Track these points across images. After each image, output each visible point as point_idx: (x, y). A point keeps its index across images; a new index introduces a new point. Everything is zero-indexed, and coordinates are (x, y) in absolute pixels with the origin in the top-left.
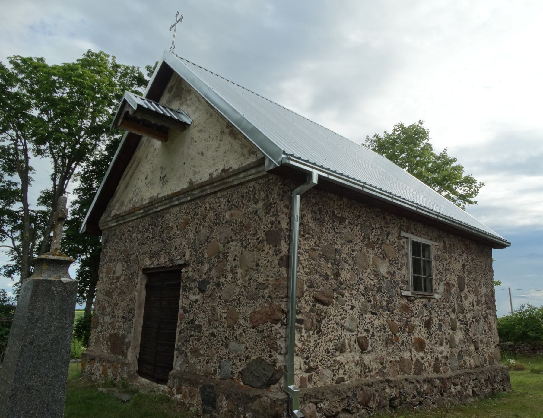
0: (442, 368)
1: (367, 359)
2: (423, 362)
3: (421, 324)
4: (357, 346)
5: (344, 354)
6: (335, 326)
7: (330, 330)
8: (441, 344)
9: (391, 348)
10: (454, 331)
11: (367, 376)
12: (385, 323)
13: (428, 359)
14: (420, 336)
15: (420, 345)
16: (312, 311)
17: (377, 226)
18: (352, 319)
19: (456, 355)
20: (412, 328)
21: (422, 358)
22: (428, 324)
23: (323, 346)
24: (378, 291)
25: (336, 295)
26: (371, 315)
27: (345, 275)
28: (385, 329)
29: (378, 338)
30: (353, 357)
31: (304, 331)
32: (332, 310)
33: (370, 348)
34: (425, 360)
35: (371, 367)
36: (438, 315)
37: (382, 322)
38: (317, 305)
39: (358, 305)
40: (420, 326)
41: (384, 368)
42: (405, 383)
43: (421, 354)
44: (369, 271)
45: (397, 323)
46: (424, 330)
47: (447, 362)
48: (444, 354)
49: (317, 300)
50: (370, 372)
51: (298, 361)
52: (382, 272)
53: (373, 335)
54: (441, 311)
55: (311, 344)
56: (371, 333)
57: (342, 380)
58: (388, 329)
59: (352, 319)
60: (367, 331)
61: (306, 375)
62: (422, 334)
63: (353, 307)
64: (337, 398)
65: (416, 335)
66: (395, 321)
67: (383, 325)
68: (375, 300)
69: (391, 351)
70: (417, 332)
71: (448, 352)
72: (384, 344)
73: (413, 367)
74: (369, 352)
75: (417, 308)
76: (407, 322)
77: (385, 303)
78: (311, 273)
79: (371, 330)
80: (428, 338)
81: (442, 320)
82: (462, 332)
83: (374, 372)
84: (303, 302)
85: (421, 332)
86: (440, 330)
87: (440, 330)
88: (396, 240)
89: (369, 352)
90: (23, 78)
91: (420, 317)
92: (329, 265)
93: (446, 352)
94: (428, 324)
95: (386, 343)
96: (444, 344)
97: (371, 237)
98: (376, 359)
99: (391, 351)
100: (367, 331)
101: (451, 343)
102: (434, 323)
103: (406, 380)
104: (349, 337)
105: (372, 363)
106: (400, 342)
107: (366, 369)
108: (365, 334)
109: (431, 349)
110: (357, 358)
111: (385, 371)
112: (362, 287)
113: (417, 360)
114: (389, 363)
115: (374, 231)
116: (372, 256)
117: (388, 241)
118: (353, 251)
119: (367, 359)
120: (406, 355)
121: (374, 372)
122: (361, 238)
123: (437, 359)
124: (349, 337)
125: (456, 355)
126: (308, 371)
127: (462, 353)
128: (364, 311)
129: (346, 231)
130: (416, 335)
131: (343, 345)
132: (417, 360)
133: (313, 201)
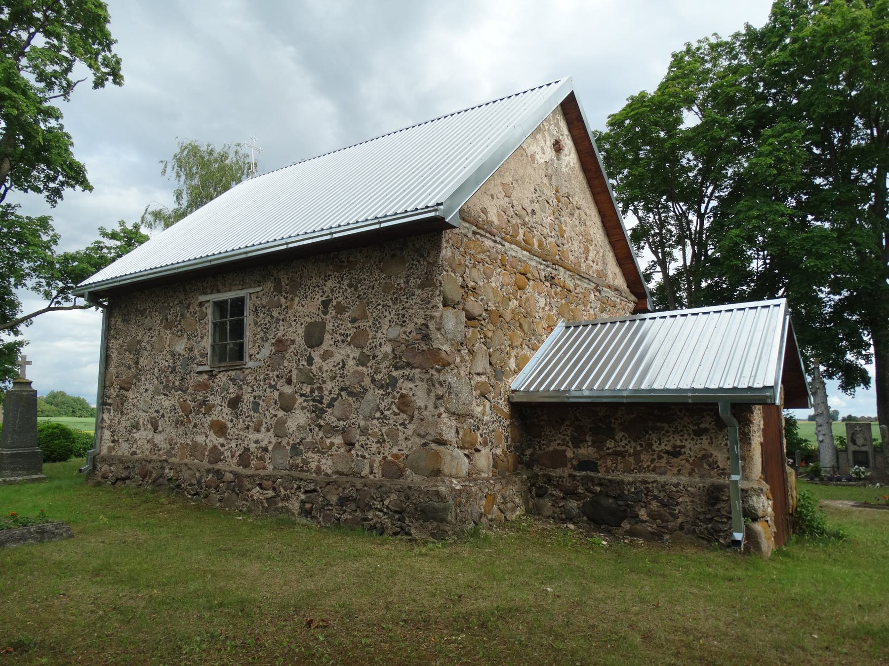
0: (254, 462)
1: (159, 439)
2: (222, 449)
3: (223, 404)
4: (149, 426)
5: (139, 432)
6: (132, 407)
7: (129, 411)
8: (258, 431)
9: (181, 430)
10: (287, 412)
11: (155, 454)
12: (177, 404)
13: (230, 448)
14: (220, 418)
15: (220, 429)
16: (117, 396)
17: (176, 302)
18: (145, 401)
19: (289, 448)
20: (209, 409)
21: (223, 445)
22: (234, 403)
23: (124, 424)
24: (171, 372)
25: (134, 381)
26: (163, 396)
27: (143, 362)
28: (175, 409)
29: (167, 419)
30: (147, 435)
31: (112, 411)
32: (130, 394)
33: (160, 429)
34: (226, 448)
35: (160, 446)
36: (253, 390)
37: (173, 403)
38: (121, 391)
39: (151, 388)
40: (221, 406)
41: (173, 449)
42: (184, 468)
43: (222, 440)
44: (164, 353)
45: (190, 403)
46: (226, 410)
47: (266, 456)
48: (263, 444)
49: (121, 388)
50: (159, 450)
51: (107, 434)
52: (178, 350)
53: (163, 416)
54: (259, 384)
55: (116, 422)
56: (161, 414)
57: (134, 453)
58: (179, 410)
59: (145, 401)
60: (157, 411)
61: (112, 445)
62: (224, 415)
63: (146, 390)
64: (121, 466)
65: (215, 416)
66: (188, 401)
67: (174, 406)
68: (168, 381)
69: (181, 433)
70: (216, 413)
71: (270, 442)
72: (174, 424)
73: (206, 453)
74: (160, 432)
75: (219, 383)
76: (204, 402)
77: (177, 383)
78: (119, 366)
79: (161, 411)
80: (232, 421)
81: (260, 397)
82: (305, 414)
83: (162, 451)
84: (112, 390)
85: (222, 413)
86: (256, 410)
87: (256, 410)
88: (197, 309)
89: (160, 432)
90: (806, 87)
91: (223, 395)
92: (132, 356)
93: (266, 442)
94: (234, 403)
95: (177, 424)
96: (263, 429)
97: (169, 317)
98: (166, 439)
99: (181, 433)
100: (157, 411)
101: (279, 429)
102: (245, 401)
103: (186, 464)
104: (143, 417)
105: (162, 443)
106: (193, 424)
107: (155, 447)
108: (155, 414)
109: (238, 435)
110: (150, 437)
111: (173, 452)
112: (156, 370)
113: (215, 447)
114: (179, 445)
115: (172, 309)
116: (168, 337)
117: (188, 314)
118: (152, 338)
119: (159, 439)
120: (200, 439)
121: (162, 451)
122: (159, 322)
123: (247, 449)
124: (143, 417)
125: (287, 447)
126: (113, 441)
127: (301, 447)
128: (156, 392)
129: (147, 320)
130: (215, 416)
131: (138, 423)
132: (215, 447)
133: (123, 306)
